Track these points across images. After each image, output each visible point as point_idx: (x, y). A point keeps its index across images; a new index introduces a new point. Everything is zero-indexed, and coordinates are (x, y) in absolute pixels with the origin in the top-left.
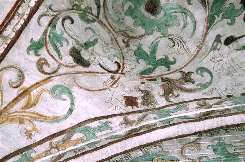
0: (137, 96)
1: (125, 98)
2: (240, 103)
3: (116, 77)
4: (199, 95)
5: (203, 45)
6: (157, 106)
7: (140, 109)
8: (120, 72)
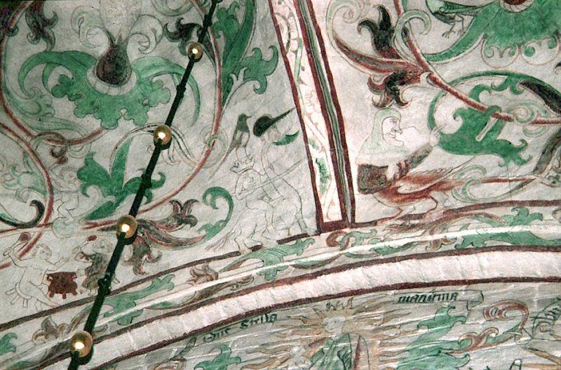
0: (75, 270)
1: (51, 278)
2: (271, 263)
3: (32, 234)
4: (199, 252)
5: (217, 138)
7: (79, 297)
8: (42, 222)
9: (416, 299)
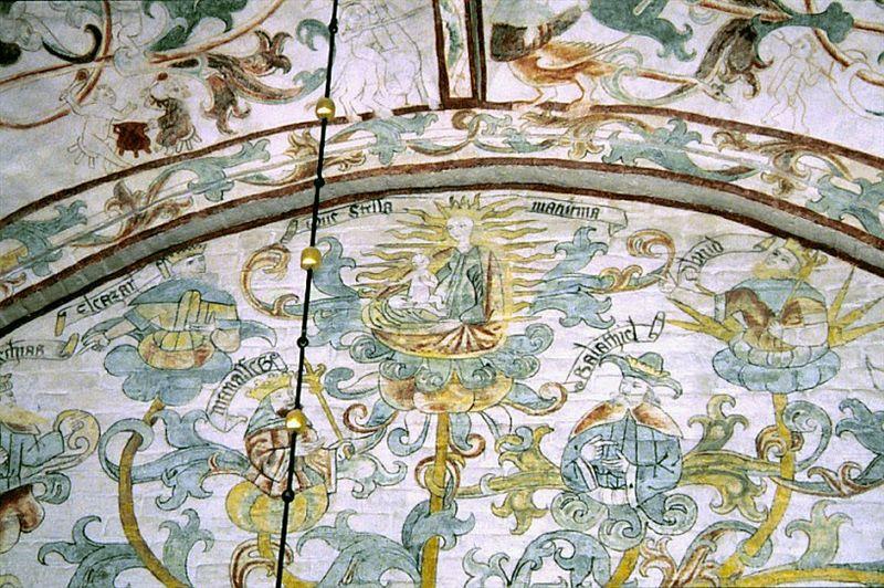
1: (118, 130)
6: (198, 147)
9: (552, 209)
